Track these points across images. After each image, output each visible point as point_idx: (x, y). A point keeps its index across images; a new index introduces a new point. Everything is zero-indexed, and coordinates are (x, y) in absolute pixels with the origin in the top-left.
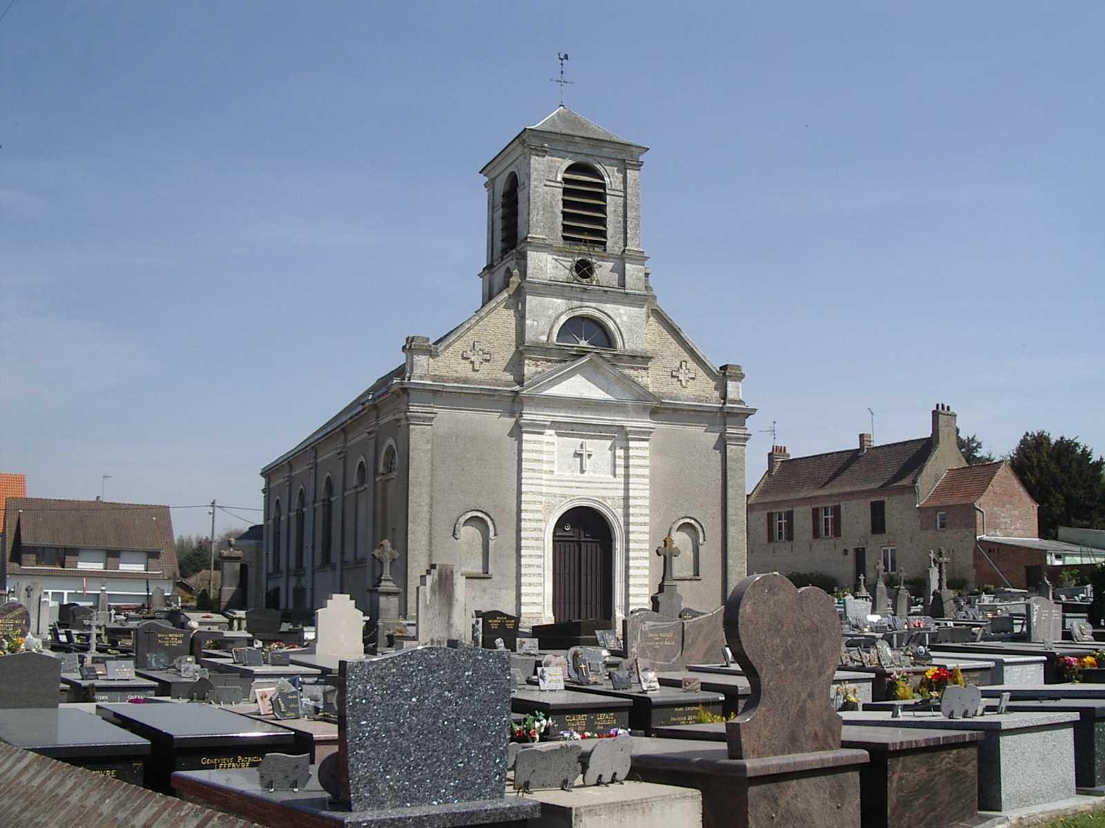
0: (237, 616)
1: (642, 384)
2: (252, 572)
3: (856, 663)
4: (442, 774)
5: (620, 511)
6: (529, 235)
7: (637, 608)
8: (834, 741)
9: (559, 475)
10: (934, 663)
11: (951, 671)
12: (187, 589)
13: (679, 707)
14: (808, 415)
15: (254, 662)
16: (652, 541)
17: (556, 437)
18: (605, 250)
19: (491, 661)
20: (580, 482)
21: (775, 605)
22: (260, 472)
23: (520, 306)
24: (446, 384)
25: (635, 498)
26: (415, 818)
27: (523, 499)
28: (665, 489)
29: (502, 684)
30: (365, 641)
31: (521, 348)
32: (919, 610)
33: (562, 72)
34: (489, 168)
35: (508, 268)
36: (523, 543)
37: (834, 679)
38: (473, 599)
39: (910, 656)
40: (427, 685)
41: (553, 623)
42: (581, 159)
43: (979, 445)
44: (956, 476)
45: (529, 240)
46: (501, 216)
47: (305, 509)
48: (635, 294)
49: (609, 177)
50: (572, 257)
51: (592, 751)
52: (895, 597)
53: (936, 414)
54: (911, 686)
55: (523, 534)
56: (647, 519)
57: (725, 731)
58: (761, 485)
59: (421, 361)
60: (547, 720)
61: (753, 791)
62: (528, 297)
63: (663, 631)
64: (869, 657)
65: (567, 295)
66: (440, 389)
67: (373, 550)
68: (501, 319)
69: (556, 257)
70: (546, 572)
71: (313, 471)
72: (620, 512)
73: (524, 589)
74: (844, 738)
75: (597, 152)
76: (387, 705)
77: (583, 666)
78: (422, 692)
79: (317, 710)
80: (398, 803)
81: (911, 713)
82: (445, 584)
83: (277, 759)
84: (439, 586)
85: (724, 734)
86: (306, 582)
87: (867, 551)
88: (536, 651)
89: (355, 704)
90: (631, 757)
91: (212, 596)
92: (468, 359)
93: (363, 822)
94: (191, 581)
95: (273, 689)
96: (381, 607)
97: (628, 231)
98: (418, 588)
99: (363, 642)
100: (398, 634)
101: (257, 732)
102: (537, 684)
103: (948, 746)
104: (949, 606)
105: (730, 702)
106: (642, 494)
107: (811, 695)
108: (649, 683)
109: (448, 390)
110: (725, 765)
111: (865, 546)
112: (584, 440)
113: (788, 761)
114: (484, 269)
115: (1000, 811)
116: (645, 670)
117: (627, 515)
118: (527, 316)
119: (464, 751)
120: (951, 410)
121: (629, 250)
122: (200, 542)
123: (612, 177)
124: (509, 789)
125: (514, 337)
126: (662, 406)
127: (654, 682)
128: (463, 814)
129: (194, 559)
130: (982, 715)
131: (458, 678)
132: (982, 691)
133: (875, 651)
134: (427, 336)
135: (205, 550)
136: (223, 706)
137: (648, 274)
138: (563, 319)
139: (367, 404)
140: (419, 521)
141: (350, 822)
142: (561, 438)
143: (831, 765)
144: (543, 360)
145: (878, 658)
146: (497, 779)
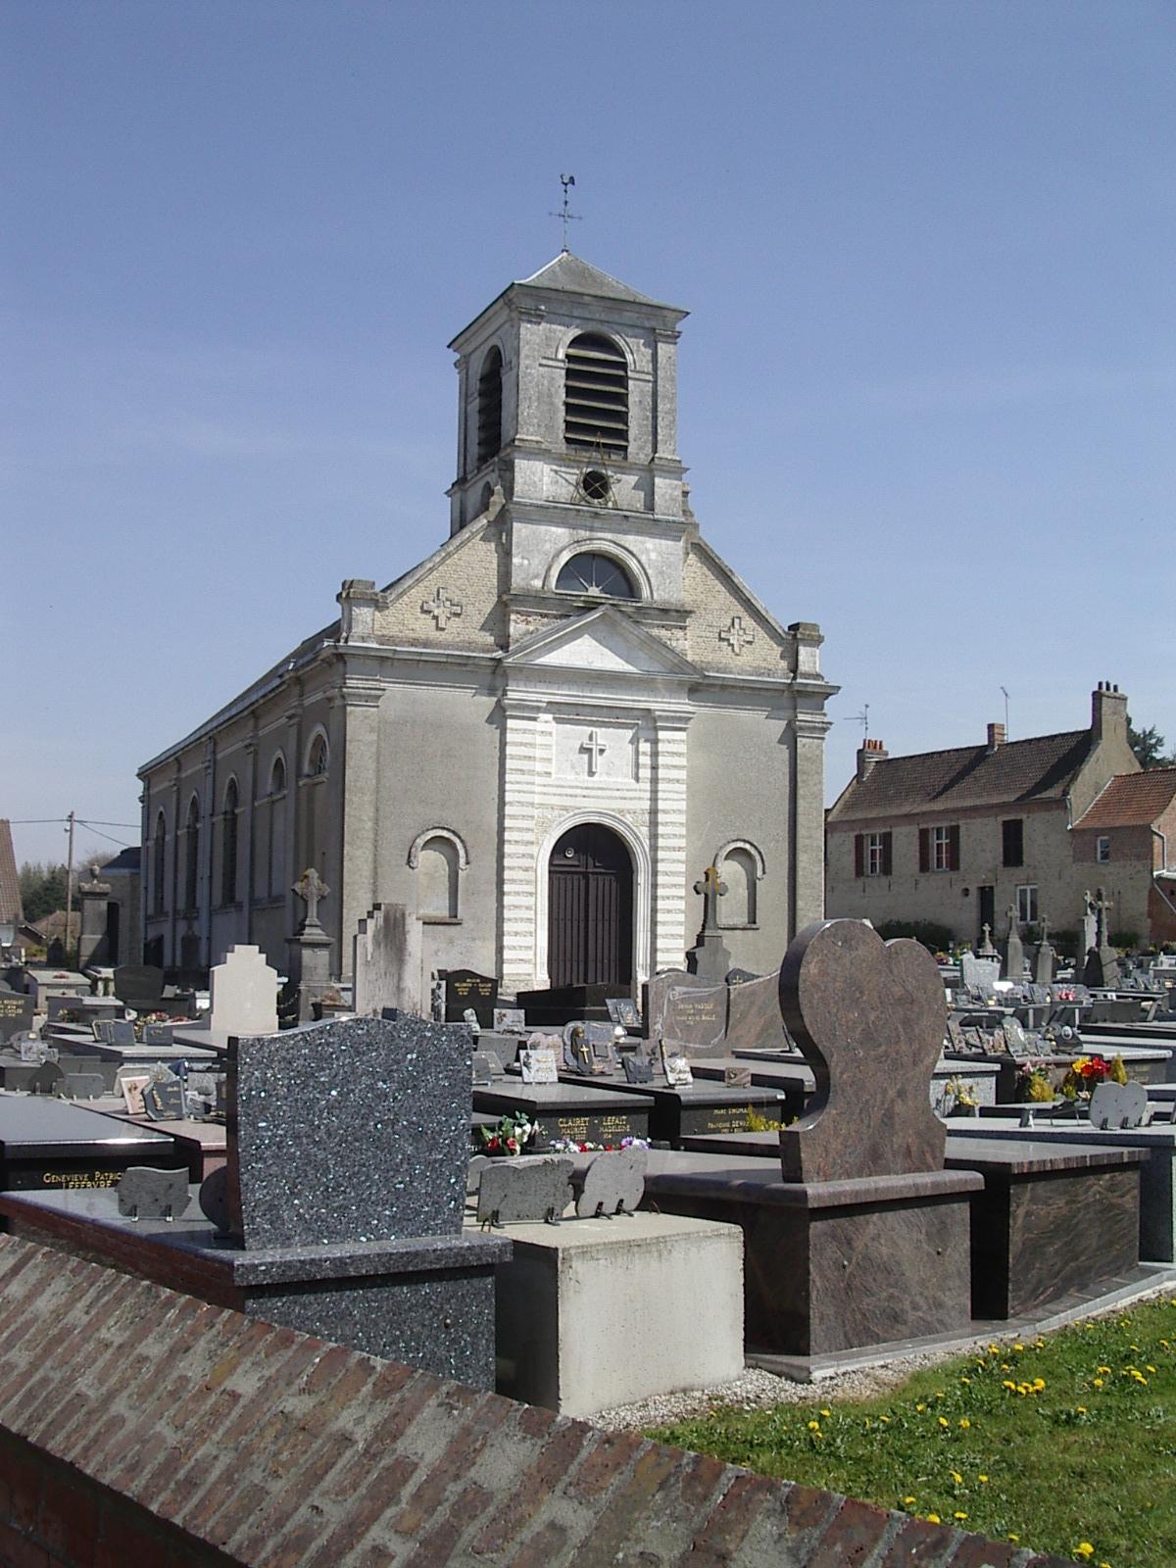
0: (103, 976)
1: (678, 650)
2: (124, 913)
3: (973, 1049)
4: (373, 1198)
5: (645, 830)
6: (518, 436)
7: (666, 968)
8: (934, 1158)
9: (558, 779)
10: (1084, 1051)
11: (1109, 1062)
12: (36, 937)
13: (719, 1109)
14: (924, 691)
15: (121, 1040)
16: (688, 874)
17: (554, 724)
18: (625, 458)
19: (444, 1038)
20: (587, 788)
21: (851, 963)
22: (137, 771)
23: (504, 537)
24: (398, 649)
25: (665, 812)
26: (333, 1261)
27: (507, 812)
28: (707, 800)
29: (459, 1071)
30: (279, 1012)
31: (505, 597)
32: (1069, 976)
33: (566, 202)
34: (460, 340)
35: (488, 483)
36: (507, 875)
37: (936, 1071)
38: (436, 953)
39: (1051, 1040)
40: (353, 1073)
41: (548, 987)
42: (591, 327)
43: (1160, 741)
44: (1125, 785)
45: (517, 443)
46: (477, 409)
47: (198, 826)
48: (668, 522)
49: (632, 353)
50: (578, 468)
51: (589, 1168)
52: (1034, 958)
53: (1097, 697)
54: (1051, 1083)
55: (507, 862)
56: (683, 843)
57: (778, 1143)
58: (847, 795)
59: (363, 614)
60: (532, 1124)
61: (816, 1228)
62: (515, 524)
63: (700, 1000)
64: (993, 1041)
65: (571, 521)
66: (390, 655)
67: (294, 882)
68: (478, 555)
69: (555, 467)
70: (539, 916)
71: (210, 771)
72: (644, 832)
73: (507, 941)
74: (947, 1155)
75: (616, 318)
76: (296, 1100)
77: (585, 1049)
78: (345, 1082)
79: (207, 1108)
80: (310, 1239)
81: (1048, 1121)
82: (393, 933)
83: (141, 1174)
84: (386, 936)
85: (776, 1146)
86: (200, 928)
87: (996, 891)
88: (521, 1027)
89: (250, 1097)
90: (645, 1178)
91: (68, 949)
92: (430, 612)
93: (261, 1265)
94: (41, 927)
95: (147, 1077)
96: (304, 964)
97: (659, 430)
98: (355, 937)
99: (278, 1013)
100: (328, 1002)
101: (125, 1139)
102: (520, 1074)
103: (1097, 1168)
104: (1111, 970)
105: (795, 1102)
106: (675, 806)
107: (901, 1094)
108: (678, 1074)
109: (401, 657)
110: (777, 1190)
111: (994, 884)
112: (594, 729)
113: (867, 1186)
114: (453, 485)
115: (1171, 1261)
116: (673, 1055)
117: (654, 837)
118: (514, 551)
119: (405, 1166)
120: (1120, 691)
121: (661, 458)
122: (53, 872)
123: (636, 354)
124: (469, 1221)
125: (495, 581)
126: (706, 681)
127: (685, 1072)
128: (402, 1255)
129: (44, 895)
130: (1149, 1125)
131: (398, 1063)
132: (1149, 1091)
133: (1001, 1033)
134: (371, 580)
135: (61, 884)
136: (76, 1101)
137: (688, 493)
138: (566, 557)
139: (287, 677)
140: (358, 842)
141: (242, 1265)
142: (561, 726)
143: (928, 1193)
144: (536, 614)
145: (1006, 1042)
146: (451, 1206)
